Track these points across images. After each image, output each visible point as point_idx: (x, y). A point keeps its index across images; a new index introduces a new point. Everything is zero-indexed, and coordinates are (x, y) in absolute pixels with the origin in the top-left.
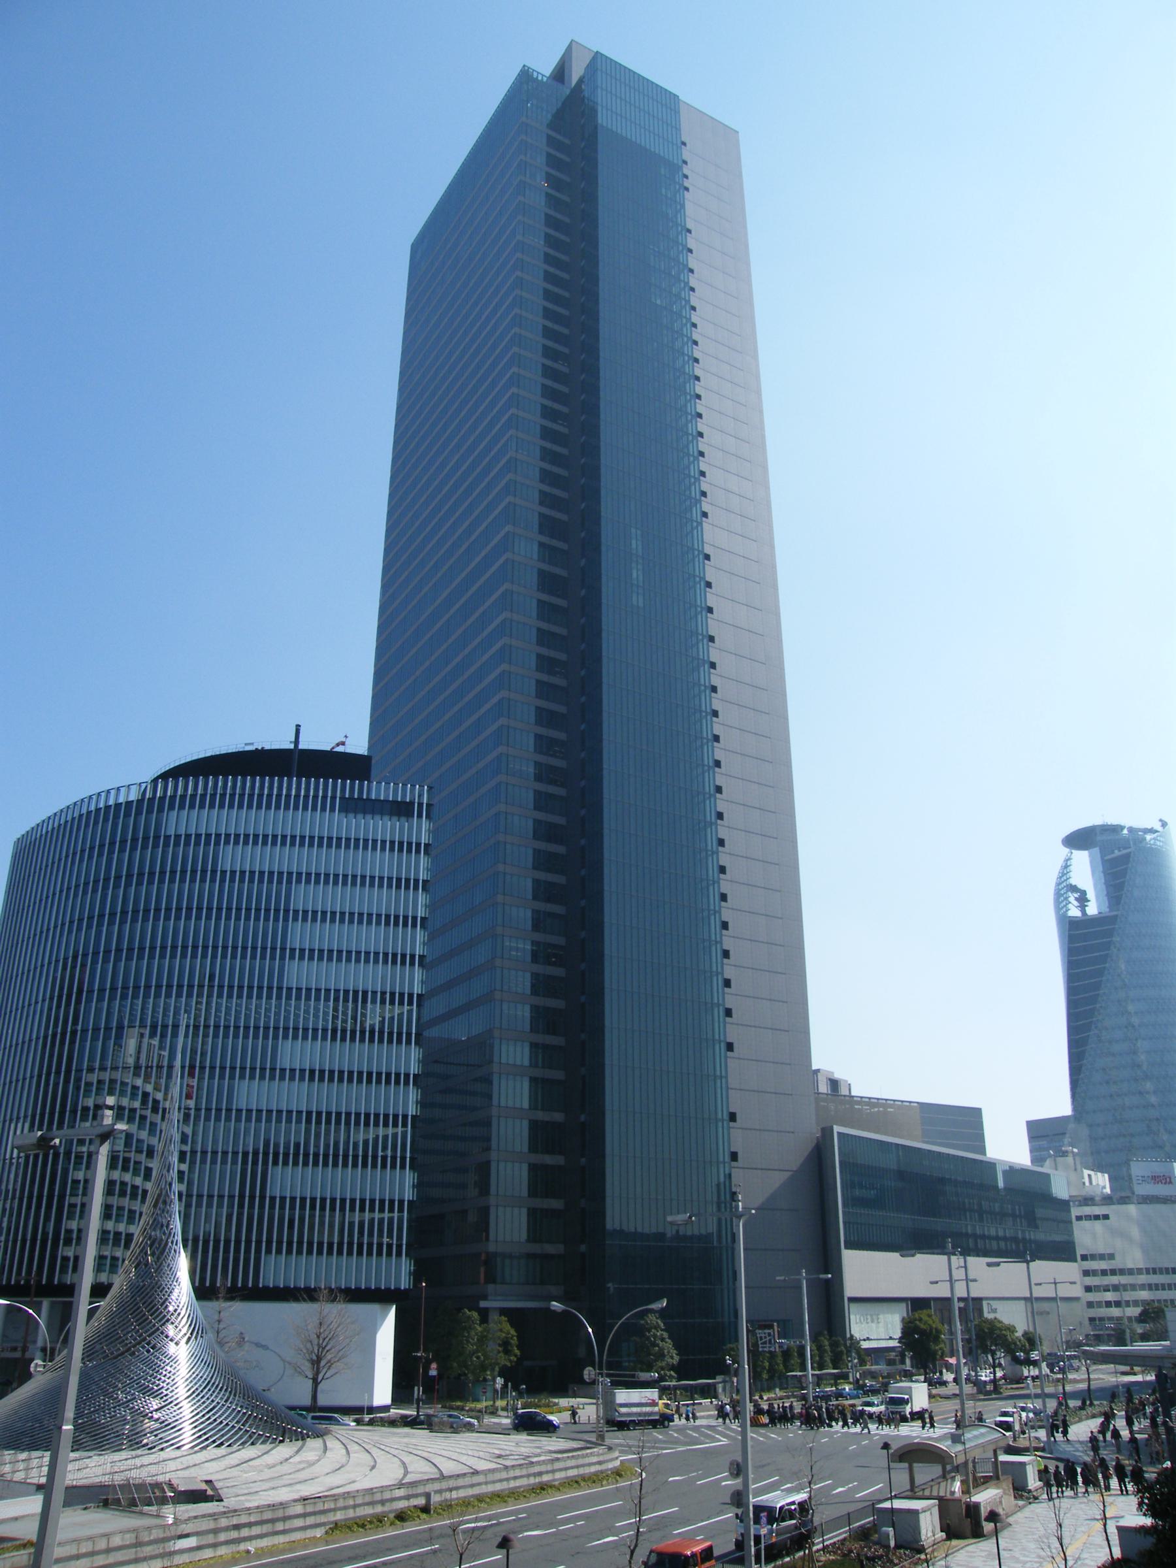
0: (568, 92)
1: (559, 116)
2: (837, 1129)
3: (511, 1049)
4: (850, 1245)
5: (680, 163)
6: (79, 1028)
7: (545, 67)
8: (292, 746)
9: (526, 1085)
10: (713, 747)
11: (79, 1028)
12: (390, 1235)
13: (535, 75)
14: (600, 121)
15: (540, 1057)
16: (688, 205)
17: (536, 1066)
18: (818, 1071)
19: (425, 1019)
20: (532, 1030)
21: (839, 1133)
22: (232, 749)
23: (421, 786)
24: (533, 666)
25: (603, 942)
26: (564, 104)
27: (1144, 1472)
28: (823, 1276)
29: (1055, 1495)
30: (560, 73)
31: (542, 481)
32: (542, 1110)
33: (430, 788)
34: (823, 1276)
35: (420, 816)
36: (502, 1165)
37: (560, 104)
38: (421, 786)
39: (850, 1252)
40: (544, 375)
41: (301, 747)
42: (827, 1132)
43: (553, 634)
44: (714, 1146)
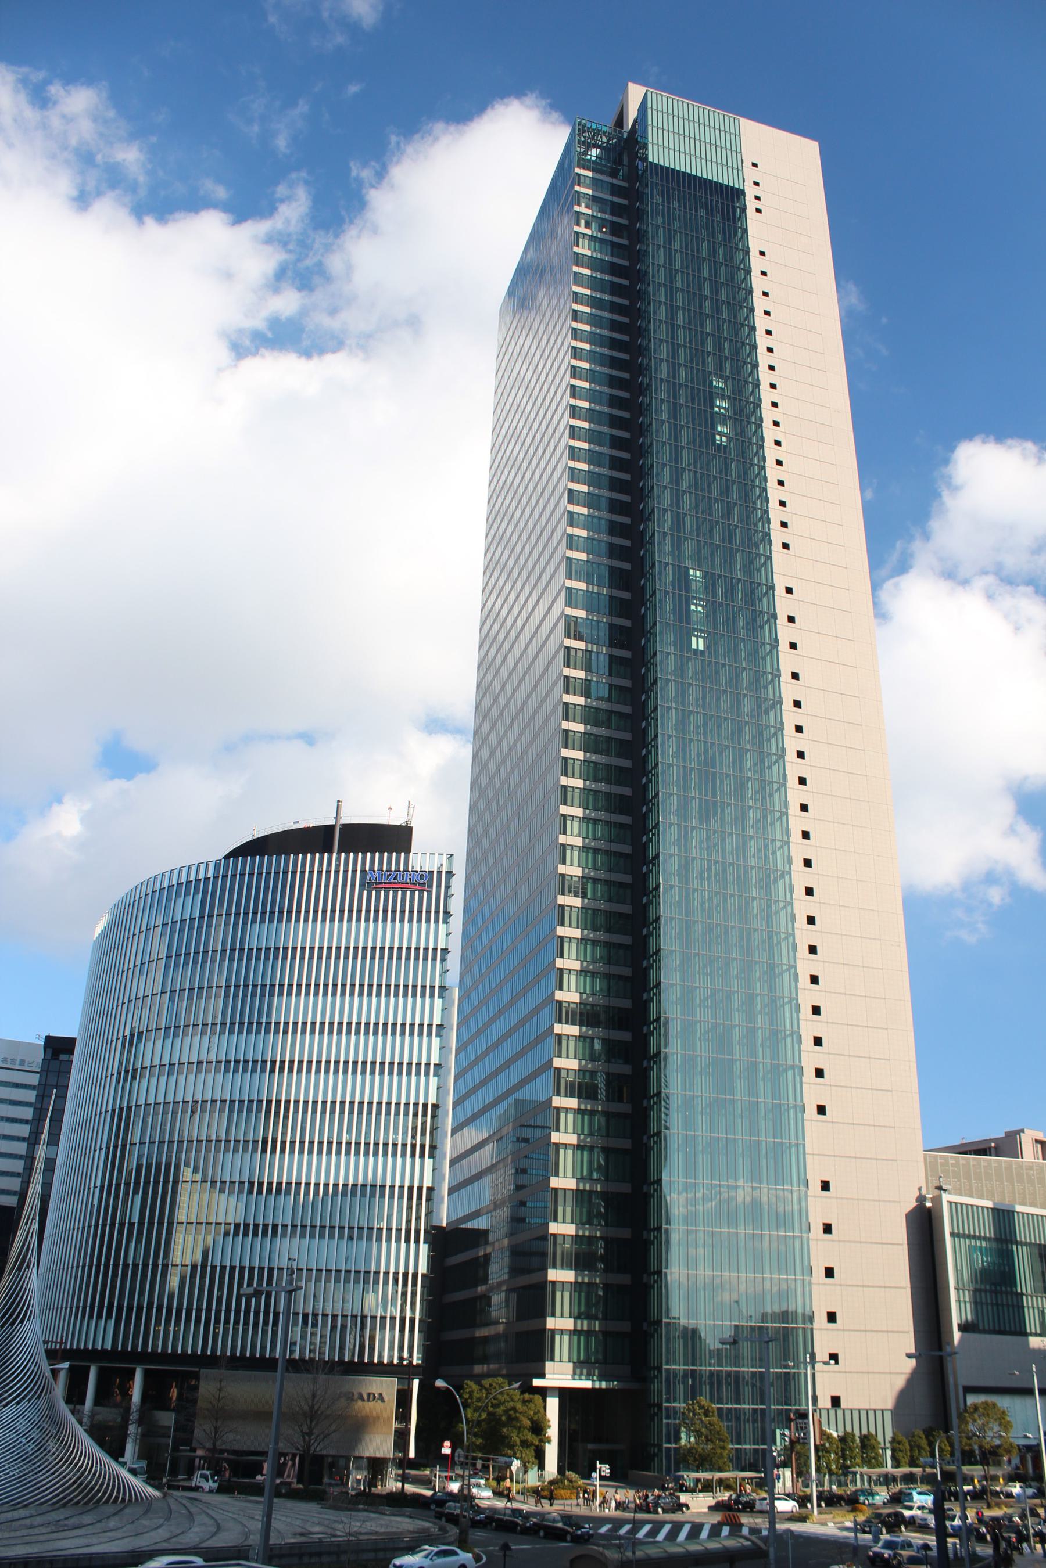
2: (946, 1197)
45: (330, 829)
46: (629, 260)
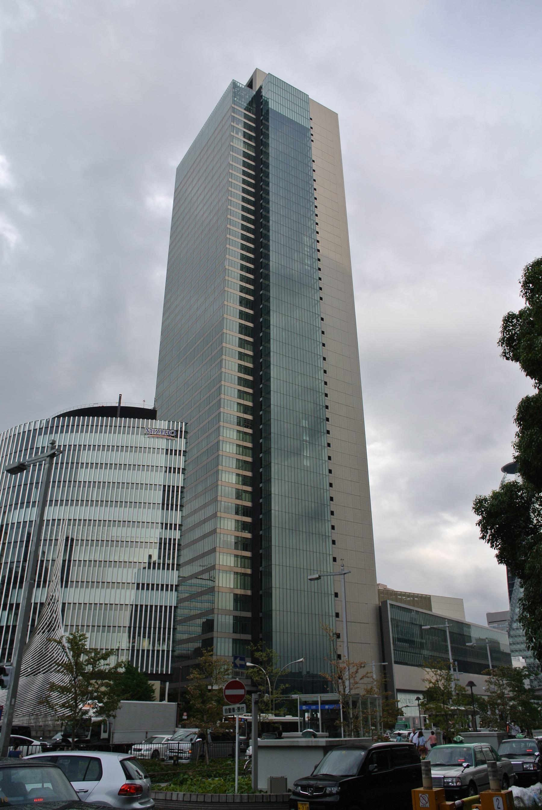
0: (254, 93)
1: (250, 104)
2: (389, 602)
3: (225, 557)
4: (396, 662)
5: (309, 128)
6: (7, 541)
7: (244, 81)
8: (117, 405)
9: (232, 576)
10: (326, 424)
11: (7, 541)
12: (169, 559)
13: (238, 84)
14: (270, 106)
15: (239, 604)
16: (313, 148)
17: (237, 610)
18: (379, 584)
19: (182, 561)
20: (233, 632)
21: (392, 605)
22: (87, 406)
23: (182, 423)
24: (236, 396)
25: (271, 553)
26: (252, 99)
27: (535, 657)
28: (383, 664)
29: (492, 686)
30: (250, 85)
31: (240, 333)
32: (240, 610)
33: (186, 424)
34: (383, 664)
35: (181, 437)
36: (220, 616)
37: (250, 99)
38: (182, 423)
39: (397, 665)
40: (241, 304)
41: (121, 405)
42: (385, 603)
43: (246, 393)
44: (327, 610)
45: (115, 408)
46: (255, 153)
